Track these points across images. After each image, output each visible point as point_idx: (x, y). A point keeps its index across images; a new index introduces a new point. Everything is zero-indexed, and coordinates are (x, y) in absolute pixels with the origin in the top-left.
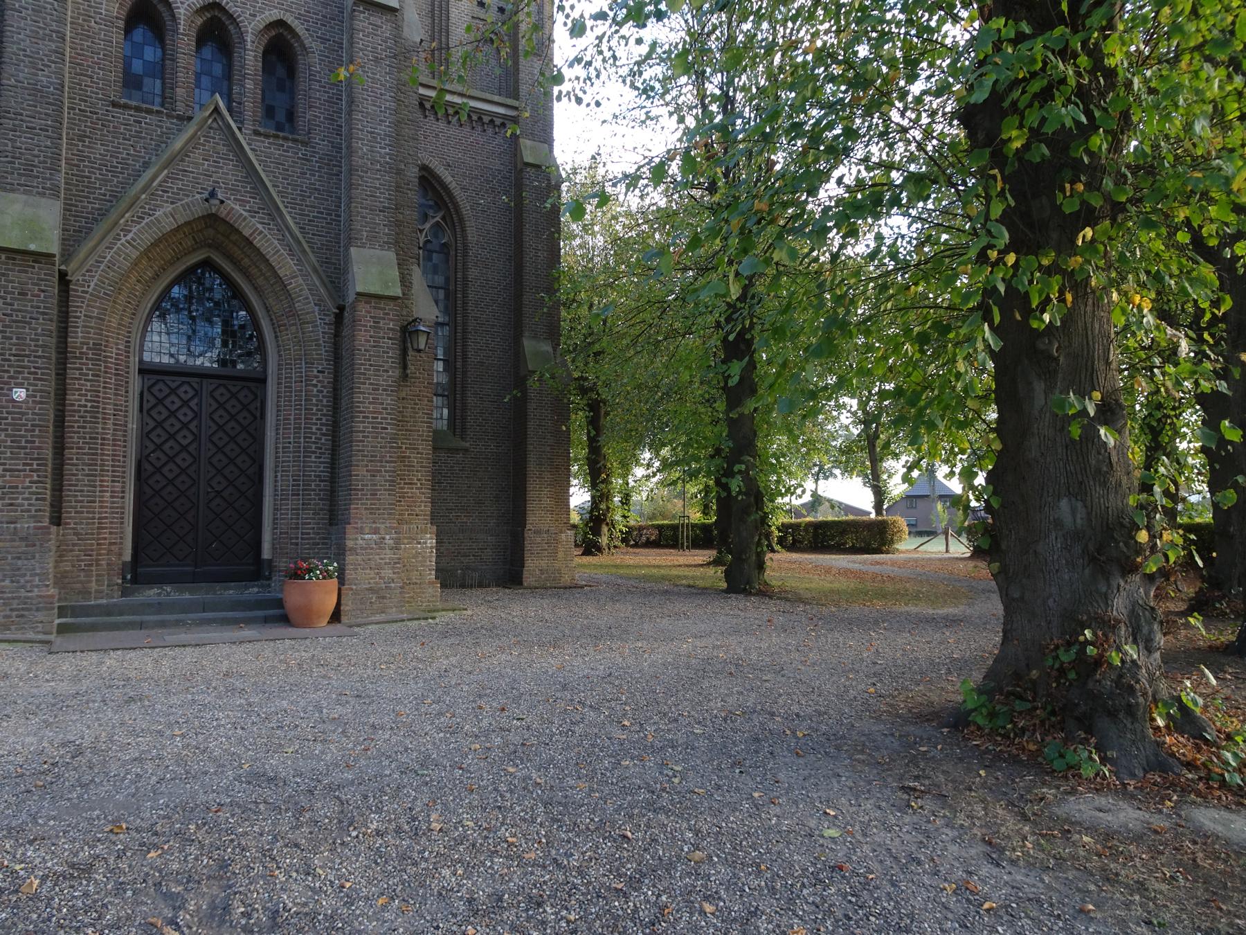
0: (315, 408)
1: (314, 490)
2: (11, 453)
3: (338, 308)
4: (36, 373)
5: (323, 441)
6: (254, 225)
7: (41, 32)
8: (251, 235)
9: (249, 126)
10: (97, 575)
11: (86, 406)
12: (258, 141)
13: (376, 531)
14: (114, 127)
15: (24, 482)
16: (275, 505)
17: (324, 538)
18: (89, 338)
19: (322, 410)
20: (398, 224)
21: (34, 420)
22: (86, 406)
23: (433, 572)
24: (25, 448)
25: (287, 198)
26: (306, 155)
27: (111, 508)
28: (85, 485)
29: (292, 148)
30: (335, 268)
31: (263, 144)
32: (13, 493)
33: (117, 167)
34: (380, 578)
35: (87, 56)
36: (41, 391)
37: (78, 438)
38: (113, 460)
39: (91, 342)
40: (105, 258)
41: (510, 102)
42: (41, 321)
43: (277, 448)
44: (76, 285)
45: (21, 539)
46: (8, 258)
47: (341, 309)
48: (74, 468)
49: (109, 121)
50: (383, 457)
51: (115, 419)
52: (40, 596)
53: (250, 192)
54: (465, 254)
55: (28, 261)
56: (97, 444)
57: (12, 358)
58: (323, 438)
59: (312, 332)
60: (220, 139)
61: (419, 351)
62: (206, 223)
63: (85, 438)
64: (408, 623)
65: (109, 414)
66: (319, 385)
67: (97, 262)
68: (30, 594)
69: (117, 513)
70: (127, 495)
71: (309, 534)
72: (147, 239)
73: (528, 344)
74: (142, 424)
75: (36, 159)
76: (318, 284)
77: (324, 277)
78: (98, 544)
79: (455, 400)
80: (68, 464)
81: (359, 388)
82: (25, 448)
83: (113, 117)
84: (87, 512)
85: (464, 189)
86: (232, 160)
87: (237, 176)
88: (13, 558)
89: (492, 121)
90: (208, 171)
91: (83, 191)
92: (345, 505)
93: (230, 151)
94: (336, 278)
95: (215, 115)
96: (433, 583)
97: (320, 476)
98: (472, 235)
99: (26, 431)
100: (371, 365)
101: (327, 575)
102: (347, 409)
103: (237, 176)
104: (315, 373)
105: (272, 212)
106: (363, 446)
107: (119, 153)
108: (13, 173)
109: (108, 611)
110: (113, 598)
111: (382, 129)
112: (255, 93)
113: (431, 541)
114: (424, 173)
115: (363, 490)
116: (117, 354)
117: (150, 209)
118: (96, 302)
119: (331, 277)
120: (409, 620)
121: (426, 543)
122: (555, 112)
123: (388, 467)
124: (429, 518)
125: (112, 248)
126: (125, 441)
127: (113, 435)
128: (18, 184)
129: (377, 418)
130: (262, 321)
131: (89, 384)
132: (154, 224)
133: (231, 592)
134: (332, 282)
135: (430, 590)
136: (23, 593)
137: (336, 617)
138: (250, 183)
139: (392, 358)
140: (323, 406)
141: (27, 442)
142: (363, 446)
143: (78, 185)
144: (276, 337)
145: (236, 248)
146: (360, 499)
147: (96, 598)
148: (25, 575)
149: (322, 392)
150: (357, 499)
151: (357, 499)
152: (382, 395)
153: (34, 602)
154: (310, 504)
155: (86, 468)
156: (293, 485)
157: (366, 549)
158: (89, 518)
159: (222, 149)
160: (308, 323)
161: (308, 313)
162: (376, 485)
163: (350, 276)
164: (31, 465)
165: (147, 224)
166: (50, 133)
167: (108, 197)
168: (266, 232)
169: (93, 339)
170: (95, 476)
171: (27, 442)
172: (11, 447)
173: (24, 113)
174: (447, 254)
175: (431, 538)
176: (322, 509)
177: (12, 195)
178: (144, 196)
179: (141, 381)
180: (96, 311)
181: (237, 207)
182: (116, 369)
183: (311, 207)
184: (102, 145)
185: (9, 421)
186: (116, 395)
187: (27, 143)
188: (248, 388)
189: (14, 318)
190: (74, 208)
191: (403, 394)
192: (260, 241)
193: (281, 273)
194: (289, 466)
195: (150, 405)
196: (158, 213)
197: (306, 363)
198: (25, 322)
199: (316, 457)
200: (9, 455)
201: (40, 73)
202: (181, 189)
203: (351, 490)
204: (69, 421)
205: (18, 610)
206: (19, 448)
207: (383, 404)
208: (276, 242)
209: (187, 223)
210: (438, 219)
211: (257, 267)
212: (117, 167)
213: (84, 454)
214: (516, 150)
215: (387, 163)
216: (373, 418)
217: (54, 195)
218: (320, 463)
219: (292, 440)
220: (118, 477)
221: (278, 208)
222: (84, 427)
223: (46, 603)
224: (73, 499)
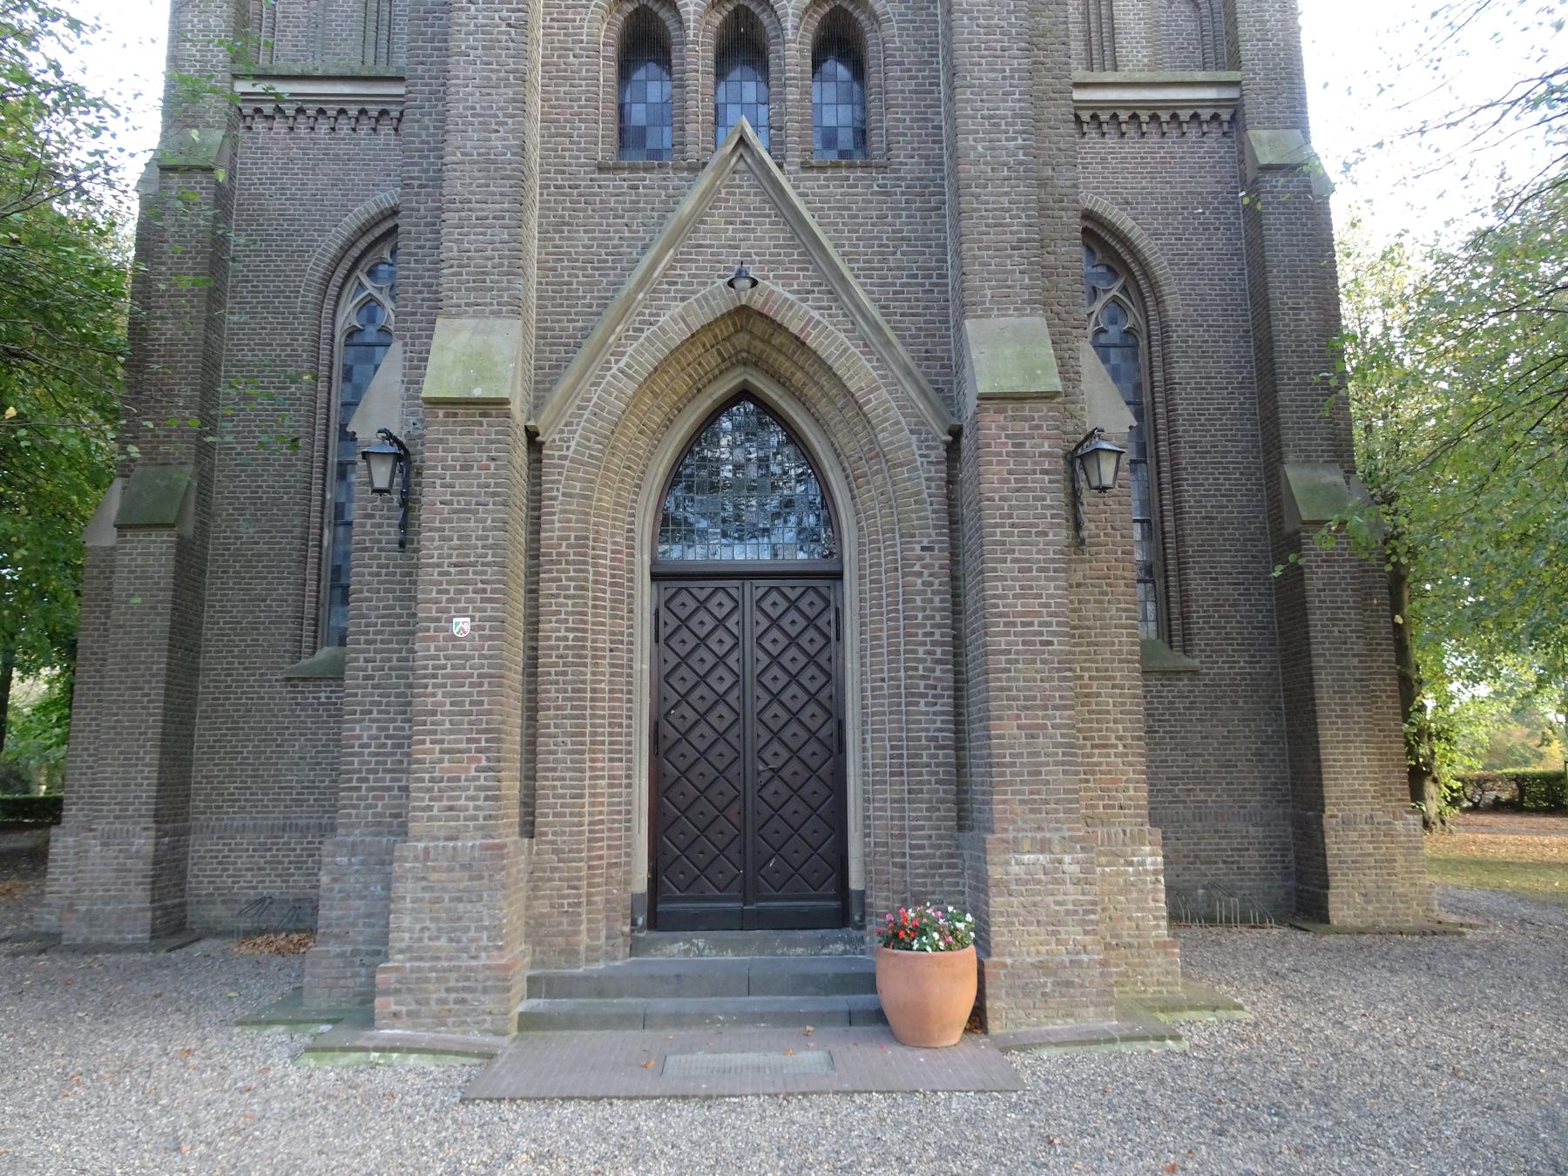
0: (920, 615)
1: (928, 765)
2: (451, 723)
3: (950, 433)
4: (484, 591)
5: (938, 674)
6: (806, 312)
7: (494, 77)
8: (802, 330)
9: (794, 159)
10: (590, 921)
11: (566, 639)
12: (809, 179)
13: (1044, 846)
14: (602, 202)
15: (467, 770)
16: (865, 792)
17: (951, 856)
18: (570, 529)
19: (933, 618)
20: (1048, 272)
21: (482, 666)
22: (566, 639)
23: (1164, 923)
24: (470, 713)
25: (857, 261)
26: (885, 186)
27: (610, 804)
28: (568, 769)
29: (864, 178)
30: (942, 367)
31: (816, 182)
32: (453, 789)
33: (607, 261)
34: (1058, 942)
35: (564, 107)
36: (491, 619)
37: (557, 691)
38: (610, 725)
39: (573, 534)
40: (589, 400)
41: (1224, 76)
42: (491, 506)
43: (863, 690)
44: (551, 448)
45: (463, 867)
46: (447, 415)
47: (956, 433)
48: (551, 741)
49: (595, 195)
50: (1049, 698)
51: (612, 658)
52: (488, 967)
53: (798, 262)
54: (1165, 341)
55: (473, 415)
56: (584, 699)
57: (452, 570)
58: (938, 668)
59: (909, 479)
60: (751, 186)
61: (1103, 489)
62: (734, 325)
63: (566, 691)
64: (1124, 1048)
65: (603, 649)
66: (926, 572)
67: (580, 408)
68: (474, 963)
69: (619, 813)
70: (635, 781)
71: (922, 847)
72: (649, 360)
73: (1296, 476)
74: (657, 661)
75: (489, 264)
76: (913, 395)
77: (924, 382)
78: (590, 868)
79: (1167, 587)
80: (543, 735)
81: (995, 570)
82: (470, 713)
83: (600, 187)
84: (572, 815)
85: (1155, 234)
86: (769, 216)
87: (778, 238)
88: (451, 900)
89: (1195, 116)
90: (734, 239)
91: (561, 305)
92: (984, 793)
93: (765, 202)
94: (944, 382)
95: (741, 150)
96: (1165, 945)
97: (936, 739)
98: (1174, 305)
99: (472, 685)
100: (1013, 525)
101: (955, 941)
102: (975, 612)
103: (778, 238)
104: (918, 551)
105: (833, 287)
106: (1009, 679)
107: (609, 239)
108: (460, 290)
109: (599, 987)
110: (615, 959)
111: (1006, 109)
112: (803, 108)
113: (1151, 858)
114: (1087, 224)
115: (1013, 764)
116: (613, 552)
117: (651, 315)
118: (578, 470)
119: (936, 382)
120: (1126, 1039)
121: (1143, 863)
122: (1306, 77)
123: (1060, 717)
124: (1145, 812)
125: (598, 384)
126: (630, 692)
127: (611, 682)
128: (467, 305)
129: (1031, 624)
130: (830, 474)
131: (570, 602)
132: (657, 336)
133: (800, 950)
134: (939, 390)
135: (1159, 960)
136: (465, 962)
137: (978, 1020)
138: (798, 247)
139: (1052, 507)
140: (933, 609)
141: (472, 703)
142: (1009, 679)
143: (554, 298)
144: (853, 498)
145: (782, 359)
146: (1011, 783)
147: (588, 961)
148: (467, 929)
149: (931, 584)
150: (1004, 783)
151: (1004, 783)
152: (1037, 579)
153: (480, 977)
154: (921, 791)
155: (568, 740)
156: (892, 757)
157: (1027, 882)
158: (574, 825)
159: (754, 201)
160: (901, 465)
161: (901, 448)
162: (1037, 754)
163: (967, 372)
164: (478, 741)
165: (648, 339)
166: (507, 221)
167: (594, 309)
168: (825, 322)
169: (575, 530)
170: (582, 752)
171: (472, 703)
172: (451, 713)
173: (473, 198)
174: (1135, 346)
175: (1153, 854)
176: (943, 801)
177: (457, 322)
178: (641, 296)
179: (655, 592)
180: (578, 484)
181: (780, 289)
182: (613, 576)
183: (898, 268)
184: (585, 231)
185: (449, 670)
186: (613, 617)
187: (477, 241)
188: (815, 589)
189: (455, 506)
190: (549, 333)
191: (1077, 577)
192: (816, 338)
193: (852, 386)
194: (883, 722)
195: (669, 630)
196: (662, 319)
197: (902, 536)
198: (469, 511)
199: (927, 704)
200: (448, 726)
201: (493, 136)
202: (694, 276)
203: (991, 765)
204: (544, 665)
205: (456, 990)
206: (462, 713)
207: (1040, 596)
208: (842, 335)
209: (707, 328)
210: (1114, 292)
211: (816, 383)
212: (607, 261)
213: (565, 717)
214: (1241, 152)
215: (1021, 163)
216: (1024, 624)
217: (512, 311)
218: (935, 713)
219: (885, 675)
220: (620, 751)
221: (842, 278)
222: (565, 673)
223: (497, 979)
224: (550, 793)
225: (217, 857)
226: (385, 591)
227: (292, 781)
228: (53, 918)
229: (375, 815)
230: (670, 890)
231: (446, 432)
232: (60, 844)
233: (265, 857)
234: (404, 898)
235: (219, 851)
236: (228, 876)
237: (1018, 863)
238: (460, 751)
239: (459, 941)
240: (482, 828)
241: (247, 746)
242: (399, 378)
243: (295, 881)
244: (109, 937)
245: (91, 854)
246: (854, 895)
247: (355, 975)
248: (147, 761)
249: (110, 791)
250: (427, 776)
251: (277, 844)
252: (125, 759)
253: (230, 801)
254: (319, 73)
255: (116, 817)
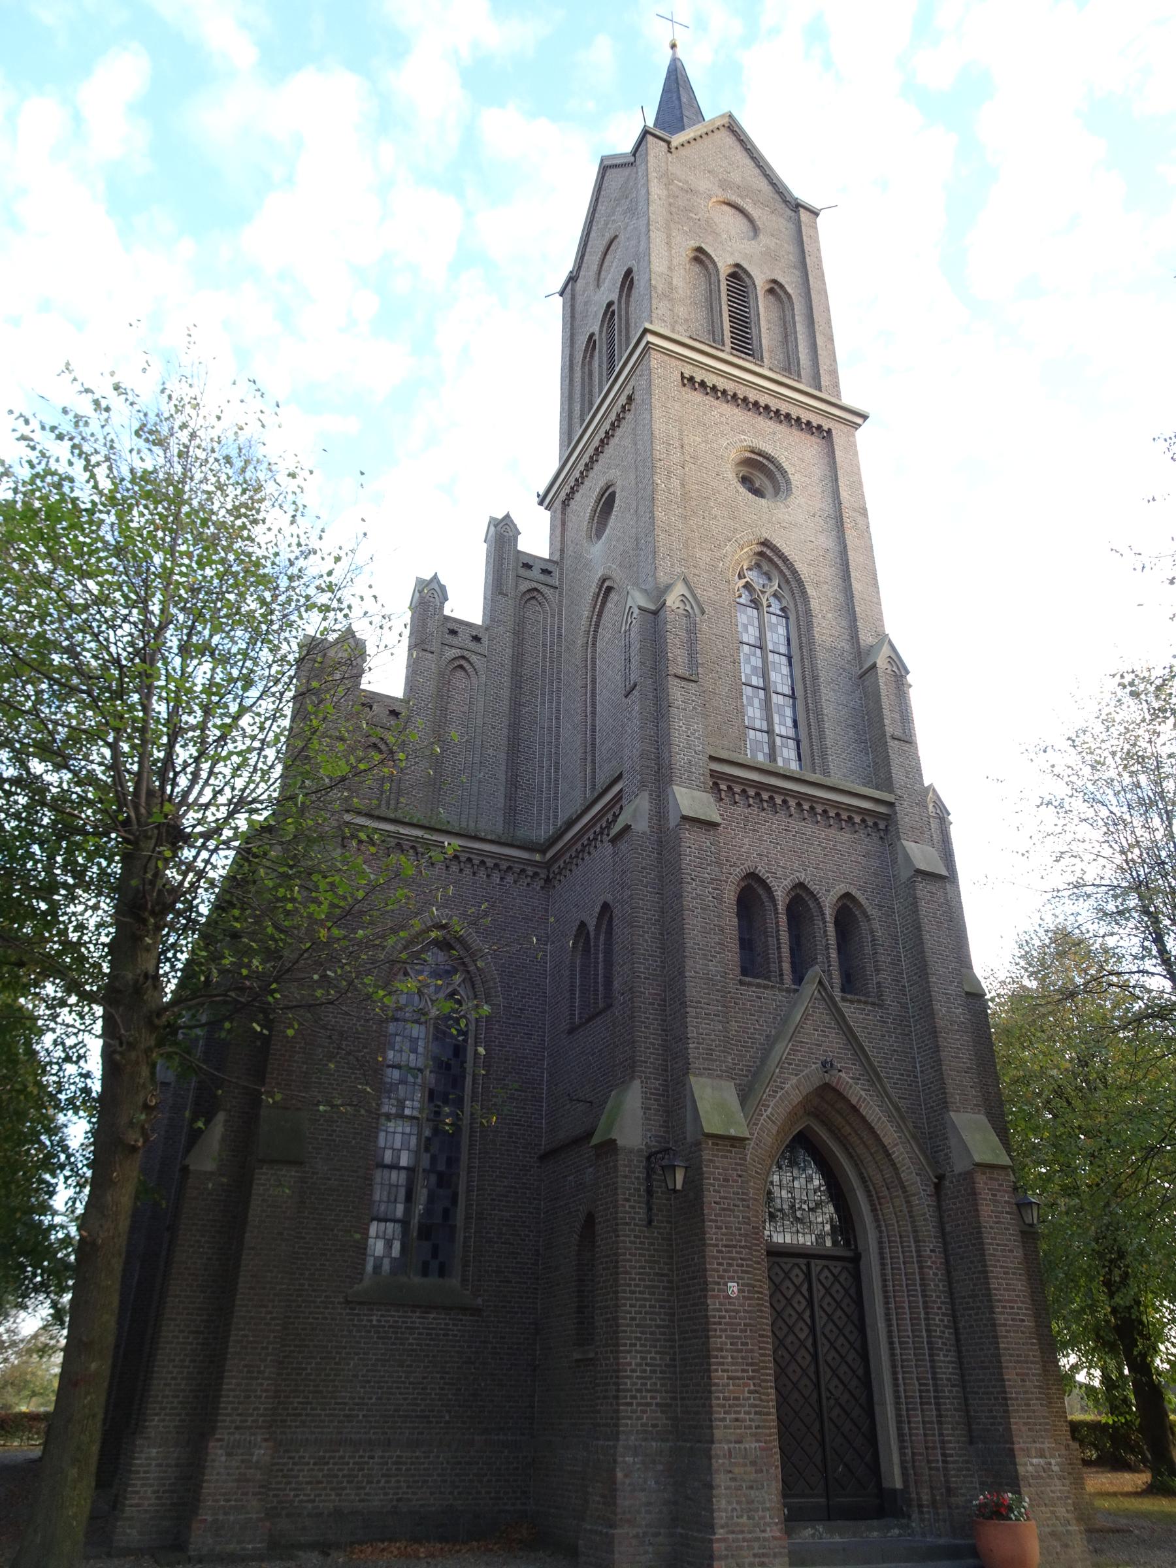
46: (713, 1144)
68: (763, 1535)
89: (469, 860)
133: (875, 1534)
148: (757, 1510)
159: (827, 1018)
164: (747, 1371)
172: (731, 1351)
188: (797, 1265)
198: (730, 1210)
200: (730, 1360)
225: (282, 1470)
226: (640, 1255)
227: (344, 1397)
228: (134, 1532)
229: (642, 1425)
231: (713, 1155)
232: (143, 1456)
233: (322, 1470)
234: (720, 1486)
235: (285, 1464)
236: (291, 1490)
237: (1032, 1464)
238: (738, 1378)
239: (753, 1519)
240: (755, 1435)
241: (310, 1363)
242: (639, 1105)
243: (347, 1495)
244: (231, 1547)
245: (217, 1464)
247: (646, 1552)
248: (266, 1375)
249: (233, 1403)
250: (721, 1395)
251: (333, 1458)
252: (248, 1372)
253: (294, 1415)
254: (406, 820)
255: (237, 1428)
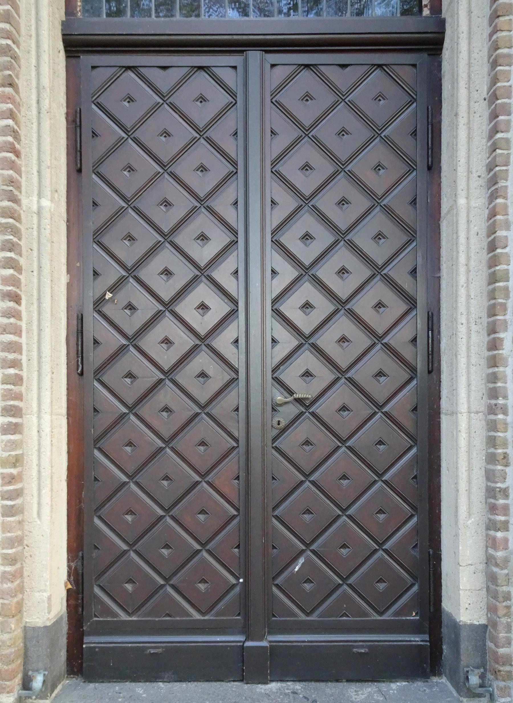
230: (109, 612)
246: (464, 634)
